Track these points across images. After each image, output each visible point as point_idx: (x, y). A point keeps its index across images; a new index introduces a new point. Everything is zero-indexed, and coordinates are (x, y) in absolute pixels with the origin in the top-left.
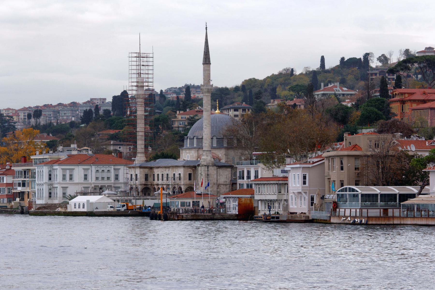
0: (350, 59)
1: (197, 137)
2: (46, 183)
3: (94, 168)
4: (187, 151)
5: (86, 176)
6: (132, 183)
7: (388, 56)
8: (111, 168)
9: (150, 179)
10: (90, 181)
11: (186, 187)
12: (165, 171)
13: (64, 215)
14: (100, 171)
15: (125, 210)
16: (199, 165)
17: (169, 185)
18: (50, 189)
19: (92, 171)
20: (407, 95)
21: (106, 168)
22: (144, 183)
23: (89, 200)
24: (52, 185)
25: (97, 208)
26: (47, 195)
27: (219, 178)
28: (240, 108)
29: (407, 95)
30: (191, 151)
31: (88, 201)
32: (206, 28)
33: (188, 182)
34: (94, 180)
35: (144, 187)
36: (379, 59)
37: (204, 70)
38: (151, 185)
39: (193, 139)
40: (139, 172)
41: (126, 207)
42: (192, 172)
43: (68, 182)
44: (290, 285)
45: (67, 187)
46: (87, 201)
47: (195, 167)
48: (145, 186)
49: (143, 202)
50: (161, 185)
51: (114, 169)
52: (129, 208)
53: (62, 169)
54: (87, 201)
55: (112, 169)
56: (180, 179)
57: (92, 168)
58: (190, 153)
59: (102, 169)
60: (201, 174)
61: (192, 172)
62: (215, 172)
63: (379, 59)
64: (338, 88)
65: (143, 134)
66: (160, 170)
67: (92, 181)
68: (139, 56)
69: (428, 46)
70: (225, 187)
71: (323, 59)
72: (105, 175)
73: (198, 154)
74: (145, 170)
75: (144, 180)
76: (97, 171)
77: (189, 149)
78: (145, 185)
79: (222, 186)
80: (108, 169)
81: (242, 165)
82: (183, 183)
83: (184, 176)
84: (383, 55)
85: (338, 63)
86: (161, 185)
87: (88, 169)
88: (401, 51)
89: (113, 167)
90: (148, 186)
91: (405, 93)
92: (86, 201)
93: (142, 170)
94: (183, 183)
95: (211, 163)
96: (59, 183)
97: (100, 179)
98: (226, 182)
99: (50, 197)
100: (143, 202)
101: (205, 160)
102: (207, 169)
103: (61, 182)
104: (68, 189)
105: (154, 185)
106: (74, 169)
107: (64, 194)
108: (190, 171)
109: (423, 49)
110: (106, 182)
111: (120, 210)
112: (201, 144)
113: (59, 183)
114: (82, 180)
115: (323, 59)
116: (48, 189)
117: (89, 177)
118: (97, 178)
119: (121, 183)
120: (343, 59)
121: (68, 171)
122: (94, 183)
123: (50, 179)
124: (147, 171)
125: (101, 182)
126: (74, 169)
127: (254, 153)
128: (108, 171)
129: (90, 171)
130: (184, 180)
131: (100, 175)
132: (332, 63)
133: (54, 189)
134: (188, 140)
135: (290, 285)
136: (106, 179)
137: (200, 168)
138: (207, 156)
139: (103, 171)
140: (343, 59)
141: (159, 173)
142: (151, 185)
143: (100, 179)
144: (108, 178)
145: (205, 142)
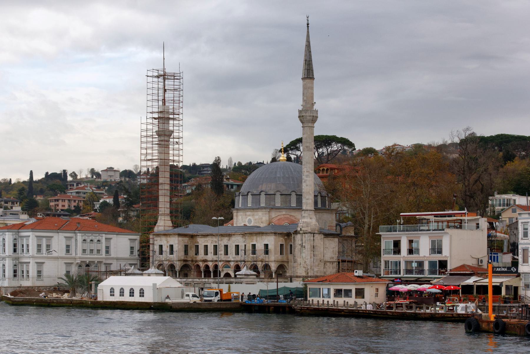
0: (53, 174)
1: (266, 192)
2: (9, 257)
3: (80, 237)
4: (248, 213)
5: (68, 246)
6: (163, 257)
7: (77, 173)
8: (102, 237)
9: (192, 252)
10: (74, 255)
11: (277, 265)
12: (221, 240)
13: (36, 305)
14: (88, 240)
15: (218, 301)
16: (296, 232)
17: (229, 261)
18: (15, 265)
19: (76, 240)
20: (336, 171)
21: (95, 238)
22: (183, 258)
23: (156, 284)
24: (17, 259)
25: (168, 297)
26: (12, 274)
27: (325, 252)
28: (9, 201)
29: (336, 171)
30: (255, 213)
31: (155, 285)
32: (308, 24)
33: (279, 257)
34: (80, 254)
35: (183, 263)
36: (71, 175)
37: (305, 88)
38: (192, 261)
39: (247, 195)
40: (176, 242)
41: (219, 296)
42: (284, 243)
43: (44, 255)
44: (81, 353)
45: (43, 263)
46: (153, 284)
47: (288, 235)
48: (185, 263)
49: (229, 287)
50: (212, 261)
51: (106, 239)
52: (224, 298)
53: (37, 236)
54: (153, 284)
55: (104, 238)
56: (267, 252)
57: (76, 236)
58: (253, 215)
59: (91, 238)
60: (302, 246)
61: (284, 243)
62: (322, 243)
63: (71, 175)
64: (89, 188)
65: (168, 187)
66: (209, 239)
67: (76, 254)
68: (164, 76)
69: (109, 167)
70: (331, 265)
71: (31, 173)
72: (94, 246)
73: (269, 216)
74: (184, 239)
75: (183, 253)
76: (84, 240)
77: (252, 209)
78: (185, 261)
79: (328, 264)
80: (98, 238)
81: (396, 231)
82: (273, 260)
83: (275, 248)
84: (74, 172)
85: (44, 176)
86: (212, 261)
87: (72, 237)
88: (88, 169)
89: (104, 235)
90: (187, 263)
91: (334, 169)
92: (152, 285)
93: (180, 239)
94: (273, 260)
95: (317, 229)
96: (33, 257)
97: (88, 251)
98: (333, 258)
99: (15, 276)
100: (229, 287)
101: (308, 224)
102: (312, 238)
103: (36, 255)
104: (44, 265)
105: (196, 261)
106: (52, 237)
107: (39, 272)
108: (281, 240)
109: (105, 168)
110: (96, 256)
111: (211, 301)
112: (272, 203)
113: (33, 257)
114: (63, 254)
115: (31, 173)
116: (12, 266)
117: (73, 248)
118: (84, 251)
119: (113, 259)
120: (47, 173)
121: (44, 240)
122: (80, 258)
123: (15, 251)
124: (186, 239)
125: (89, 256)
126: (52, 237)
127: (401, 214)
128: (99, 241)
129: (73, 240)
130: (275, 254)
131: (88, 247)
132: (38, 176)
133: (22, 266)
134: (241, 196)
135: (81, 353)
136: (95, 252)
137: (298, 237)
138: (311, 218)
139: (92, 240)
140: (47, 173)
141: (209, 244)
142: (192, 261)
143: (88, 251)
144: (98, 251)
145: (307, 197)
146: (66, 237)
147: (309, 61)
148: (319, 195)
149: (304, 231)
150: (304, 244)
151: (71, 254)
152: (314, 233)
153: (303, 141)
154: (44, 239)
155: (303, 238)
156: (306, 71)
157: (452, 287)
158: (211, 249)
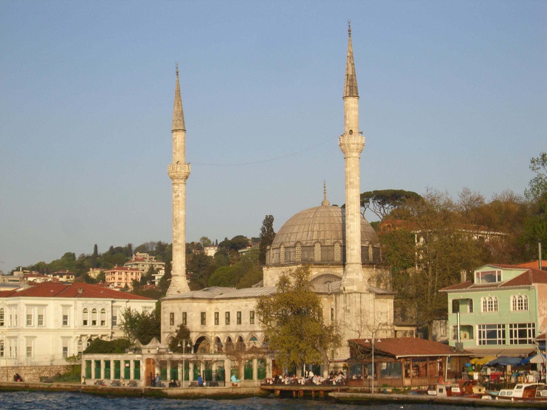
5: (65, 317)
51: (413, 331)
57: (76, 303)
71: (96, 247)
115: (96, 247)
120: (112, 247)
126: (45, 305)
138: (357, 274)
140: (112, 247)
146: (63, 306)
147: (352, 75)
148: (370, 246)
149: (348, 290)
150: (348, 308)
151: (69, 327)
152: (361, 293)
153: (425, 341)
154: (36, 308)
155: (347, 299)
156: (348, 88)
157: (272, 299)
158: (234, 317)
